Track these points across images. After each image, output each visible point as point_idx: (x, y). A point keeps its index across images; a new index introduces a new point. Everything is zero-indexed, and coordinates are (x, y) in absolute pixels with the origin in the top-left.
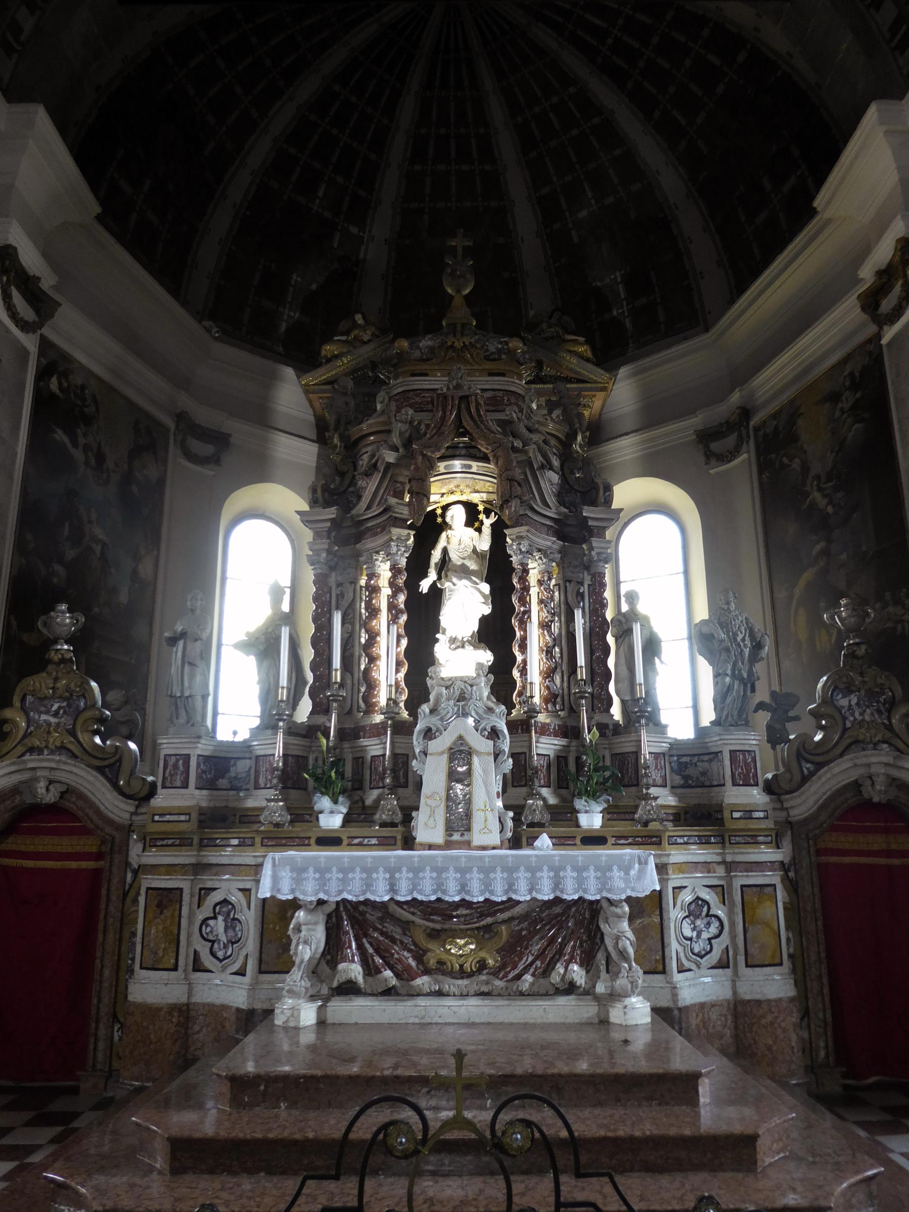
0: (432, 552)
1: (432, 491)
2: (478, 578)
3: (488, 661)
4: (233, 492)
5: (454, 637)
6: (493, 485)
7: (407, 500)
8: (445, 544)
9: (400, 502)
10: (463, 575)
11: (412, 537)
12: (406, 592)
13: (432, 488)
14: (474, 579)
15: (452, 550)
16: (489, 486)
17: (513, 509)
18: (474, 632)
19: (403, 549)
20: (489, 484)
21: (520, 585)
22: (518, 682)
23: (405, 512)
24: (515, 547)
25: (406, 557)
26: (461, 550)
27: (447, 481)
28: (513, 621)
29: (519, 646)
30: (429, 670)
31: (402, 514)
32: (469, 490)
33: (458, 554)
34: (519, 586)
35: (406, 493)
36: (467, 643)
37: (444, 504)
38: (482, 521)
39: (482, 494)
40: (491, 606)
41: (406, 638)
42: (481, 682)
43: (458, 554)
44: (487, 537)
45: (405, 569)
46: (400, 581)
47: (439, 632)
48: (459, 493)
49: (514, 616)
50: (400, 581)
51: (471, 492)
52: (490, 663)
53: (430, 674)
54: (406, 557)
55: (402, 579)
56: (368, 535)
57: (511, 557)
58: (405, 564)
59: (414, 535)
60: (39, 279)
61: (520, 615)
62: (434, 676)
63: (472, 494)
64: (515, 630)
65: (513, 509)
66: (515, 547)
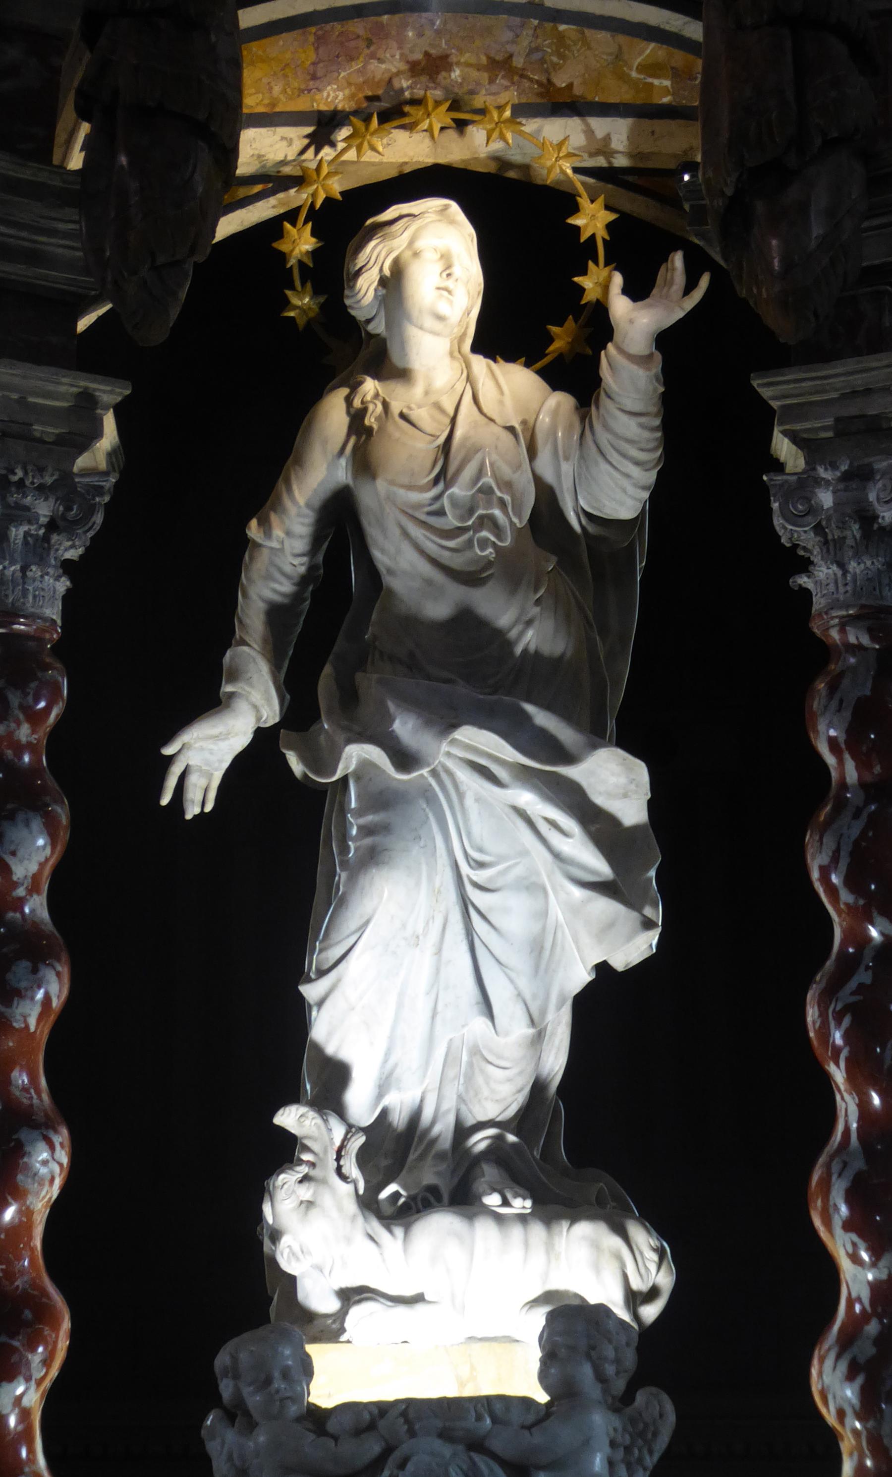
0: (253, 530)
1: (252, 102)
2: (566, 715)
3: (634, 1299)
4: (609, 318)
5: (399, 1119)
6: (679, 58)
7: (76, 161)
8: (342, 474)
9: (26, 173)
10: (462, 689)
11: (109, 423)
12: (62, 813)
13: (250, 76)
14: (542, 718)
15: (392, 516)
16: (652, 68)
17: (817, 230)
18: (538, 1087)
19: (44, 509)
20: (649, 50)
21: (862, 765)
22: (847, 1445)
23: (56, 247)
24: (826, 499)
25: (68, 567)
26: (452, 520)
27: (358, 27)
28: (812, 1014)
29: (851, 1198)
30: (222, 1360)
31: (34, 257)
32: (510, 96)
33: (431, 544)
34: (852, 773)
35: (68, 113)
36: (490, 1172)
37: (336, 187)
38: (601, 310)
39: (600, 125)
40: (656, 913)
41: (62, 1137)
42: (587, 1444)
43: (431, 544)
44: (630, 427)
45: (58, 649)
46: (24, 733)
47: (293, 1097)
48: (440, 117)
49: (821, 979)
50: (24, 733)
51: (522, 111)
52: (650, 1312)
53: (226, 1389)
54: (68, 567)
55: (35, 719)
56: (625, 1270)
57: (805, 565)
58: (53, 612)
59: (120, 411)
60: (603, 969)
61: (863, 977)
62: (254, 1400)
63: (531, 125)
64: (827, 1080)
65: (817, 230)
66: (826, 499)
